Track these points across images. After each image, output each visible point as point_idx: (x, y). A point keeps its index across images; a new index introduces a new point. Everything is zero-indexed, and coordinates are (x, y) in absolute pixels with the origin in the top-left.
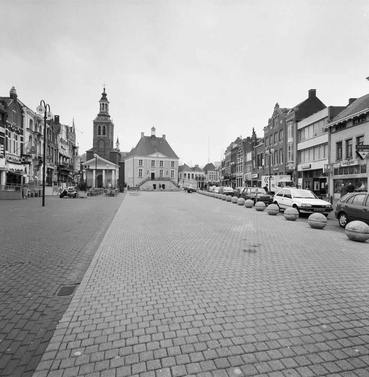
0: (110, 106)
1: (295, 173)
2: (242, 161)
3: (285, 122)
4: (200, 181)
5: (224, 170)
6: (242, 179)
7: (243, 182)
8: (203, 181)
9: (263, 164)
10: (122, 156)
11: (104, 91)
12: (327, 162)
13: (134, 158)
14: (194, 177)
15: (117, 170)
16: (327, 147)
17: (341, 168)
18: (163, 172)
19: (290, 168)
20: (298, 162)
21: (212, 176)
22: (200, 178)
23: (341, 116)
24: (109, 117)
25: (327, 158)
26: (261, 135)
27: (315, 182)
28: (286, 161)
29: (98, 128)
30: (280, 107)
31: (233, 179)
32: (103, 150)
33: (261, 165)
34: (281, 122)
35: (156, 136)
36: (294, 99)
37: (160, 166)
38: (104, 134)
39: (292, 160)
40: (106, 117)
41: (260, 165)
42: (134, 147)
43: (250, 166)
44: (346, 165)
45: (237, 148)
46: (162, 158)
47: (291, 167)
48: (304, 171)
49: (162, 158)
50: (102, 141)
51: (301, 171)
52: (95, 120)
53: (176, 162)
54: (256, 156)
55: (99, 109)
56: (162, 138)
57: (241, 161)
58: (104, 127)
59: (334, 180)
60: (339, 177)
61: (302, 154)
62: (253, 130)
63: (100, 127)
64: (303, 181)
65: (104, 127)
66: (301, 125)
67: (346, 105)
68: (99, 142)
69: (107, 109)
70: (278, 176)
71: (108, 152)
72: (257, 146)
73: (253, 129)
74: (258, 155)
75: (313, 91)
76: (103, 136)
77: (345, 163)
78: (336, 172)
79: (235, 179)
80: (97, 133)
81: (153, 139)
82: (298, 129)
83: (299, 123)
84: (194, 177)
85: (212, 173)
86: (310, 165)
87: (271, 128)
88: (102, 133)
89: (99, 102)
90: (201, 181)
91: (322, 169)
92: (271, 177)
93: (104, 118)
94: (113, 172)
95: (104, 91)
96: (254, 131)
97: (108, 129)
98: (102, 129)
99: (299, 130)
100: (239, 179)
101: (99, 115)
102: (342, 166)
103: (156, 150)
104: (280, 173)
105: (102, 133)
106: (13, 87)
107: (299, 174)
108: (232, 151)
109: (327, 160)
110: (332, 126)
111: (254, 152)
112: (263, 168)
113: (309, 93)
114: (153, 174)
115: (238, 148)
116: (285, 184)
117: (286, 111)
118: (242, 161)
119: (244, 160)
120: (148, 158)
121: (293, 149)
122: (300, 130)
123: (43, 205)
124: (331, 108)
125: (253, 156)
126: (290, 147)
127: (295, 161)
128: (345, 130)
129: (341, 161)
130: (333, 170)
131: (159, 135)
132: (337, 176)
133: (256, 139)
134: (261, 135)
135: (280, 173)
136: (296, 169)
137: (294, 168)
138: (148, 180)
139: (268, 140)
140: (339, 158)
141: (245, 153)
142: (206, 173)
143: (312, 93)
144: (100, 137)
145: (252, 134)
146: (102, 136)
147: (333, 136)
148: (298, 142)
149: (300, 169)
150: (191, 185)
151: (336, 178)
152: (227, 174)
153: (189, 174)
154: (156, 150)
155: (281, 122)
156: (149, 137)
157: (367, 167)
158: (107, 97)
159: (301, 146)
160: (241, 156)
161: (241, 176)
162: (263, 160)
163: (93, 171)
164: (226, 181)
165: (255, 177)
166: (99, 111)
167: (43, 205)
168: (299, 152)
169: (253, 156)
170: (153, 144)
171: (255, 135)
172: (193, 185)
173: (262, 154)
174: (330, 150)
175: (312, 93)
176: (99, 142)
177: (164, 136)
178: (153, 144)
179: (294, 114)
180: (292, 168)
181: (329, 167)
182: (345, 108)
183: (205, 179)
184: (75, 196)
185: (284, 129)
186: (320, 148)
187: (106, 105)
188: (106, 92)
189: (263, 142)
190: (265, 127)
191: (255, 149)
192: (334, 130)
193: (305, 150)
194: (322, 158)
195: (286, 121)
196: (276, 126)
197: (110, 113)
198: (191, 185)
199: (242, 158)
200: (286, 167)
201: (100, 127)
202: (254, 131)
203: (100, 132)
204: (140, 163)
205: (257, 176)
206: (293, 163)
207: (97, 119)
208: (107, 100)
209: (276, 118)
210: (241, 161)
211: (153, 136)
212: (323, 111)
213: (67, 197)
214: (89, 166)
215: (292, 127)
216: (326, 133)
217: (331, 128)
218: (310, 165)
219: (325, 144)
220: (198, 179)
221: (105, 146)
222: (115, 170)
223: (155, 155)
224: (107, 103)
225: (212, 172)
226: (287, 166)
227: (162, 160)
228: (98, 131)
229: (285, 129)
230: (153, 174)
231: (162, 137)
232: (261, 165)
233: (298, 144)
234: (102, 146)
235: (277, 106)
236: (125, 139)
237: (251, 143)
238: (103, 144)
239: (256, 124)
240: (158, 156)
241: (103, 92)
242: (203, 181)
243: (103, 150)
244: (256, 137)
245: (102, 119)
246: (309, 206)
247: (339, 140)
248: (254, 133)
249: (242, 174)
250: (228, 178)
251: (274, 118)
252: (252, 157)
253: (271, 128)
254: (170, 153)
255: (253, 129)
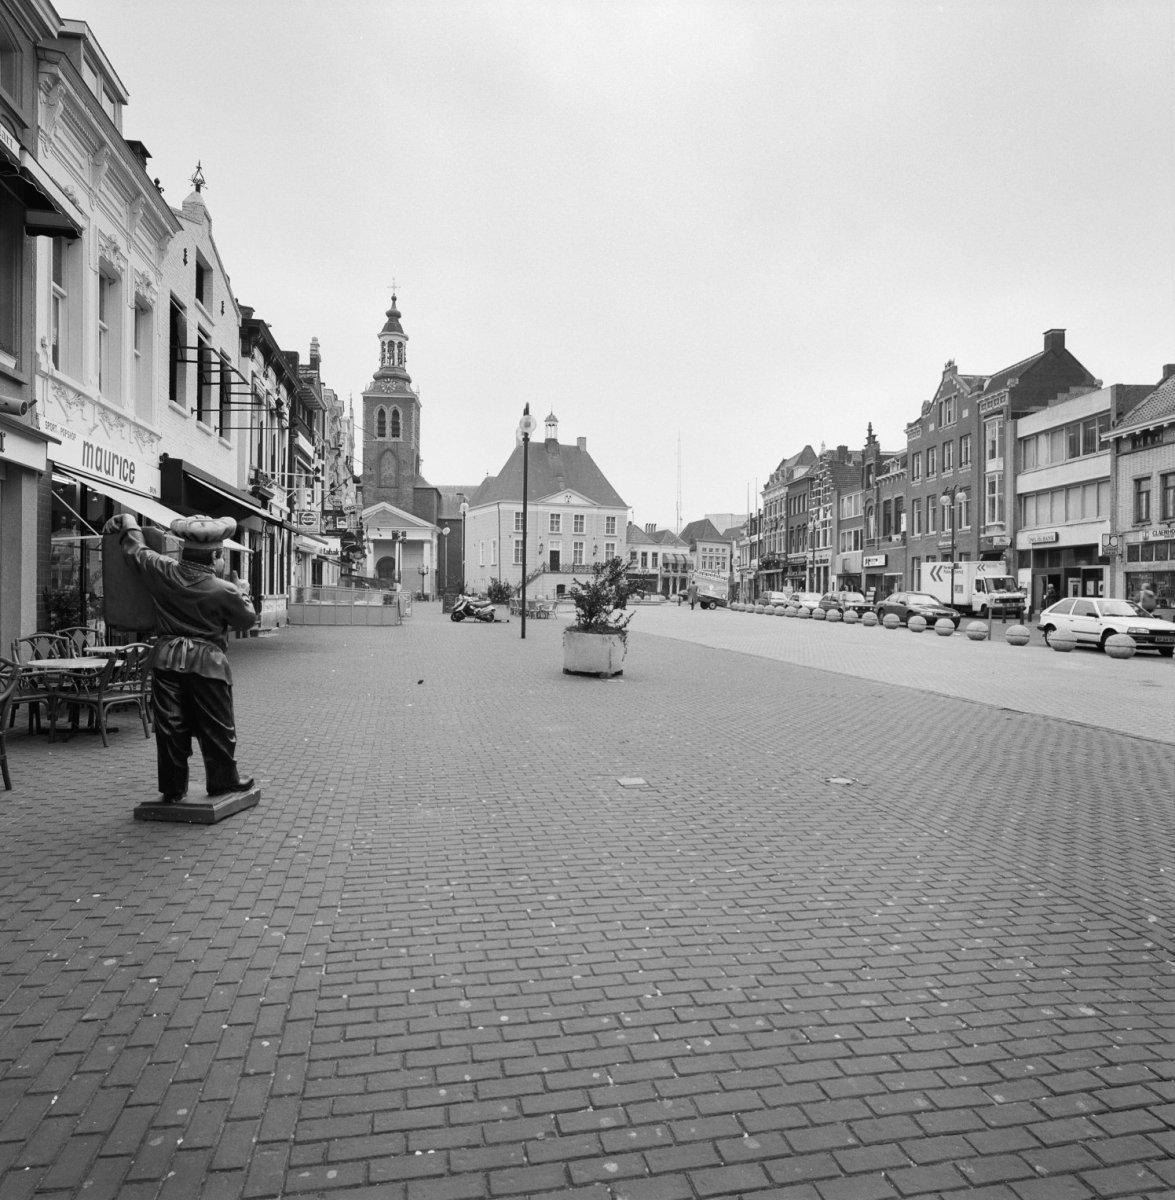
0: (409, 346)
1: (1008, 553)
2: (829, 517)
3: (979, 416)
4: (675, 575)
5: (760, 541)
6: (826, 568)
7: (833, 579)
8: (684, 575)
9: (904, 528)
10: (443, 498)
11: (394, 304)
12: (1107, 528)
13: (502, 506)
14: (660, 562)
15: (435, 541)
16: (1106, 490)
17: (1148, 544)
18: (584, 549)
19: (996, 542)
20: (1019, 525)
21: (711, 557)
22: (675, 566)
23: (1146, 412)
24: (408, 380)
25: (1106, 515)
26: (894, 442)
27: (1070, 579)
28: (981, 520)
29: (376, 417)
30: (960, 372)
31: (795, 568)
32: (392, 483)
33: (897, 531)
34: (966, 414)
35: (561, 442)
36: (1002, 347)
37: (576, 530)
38: (396, 433)
39: (1002, 518)
40: (400, 383)
41: (893, 530)
42: (495, 473)
43: (856, 533)
44: (1162, 538)
45: (809, 480)
46: (578, 506)
47: (999, 537)
48: (1035, 551)
49: (578, 506)
50: (388, 455)
51: (1028, 551)
52: (370, 391)
53: (621, 517)
54: (878, 506)
55: (379, 356)
56: (577, 448)
57: (825, 516)
58: (396, 414)
59: (1128, 574)
60: (1142, 566)
61: (1031, 504)
62: (870, 430)
63: (382, 413)
64: (1033, 576)
65: (396, 414)
66: (1027, 426)
67: (1154, 382)
68: (381, 456)
69: (402, 360)
70: (974, 564)
71: (408, 489)
72: (884, 477)
73: (870, 426)
74: (887, 503)
75: (1058, 335)
76: (394, 440)
77: (1161, 533)
78: (1133, 553)
79: (804, 568)
80: (376, 431)
81: (552, 450)
82: (1020, 435)
83: (1021, 422)
84: (660, 562)
85: (711, 550)
86: (1057, 535)
87: (932, 427)
88: (388, 430)
89: (380, 336)
90: (679, 574)
91: (1096, 546)
92: (956, 566)
93: (393, 385)
94: (427, 547)
95: (394, 304)
96: (873, 433)
97: (408, 418)
98: (388, 418)
99: (1020, 439)
100: (819, 569)
101: (377, 378)
102: (1152, 538)
103: (562, 485)
104: (961, 554)
105: (388, 430)
106: (315, 339)
107: (1022, 558)
108: (791, 486)
109: (1108, 523)
110: (1124, 436)
111: (872, 494)
112: (904, 540)
113: (1046, 339)
114: (555, 555)
115: (813, 479)
116: (992, 586)
117: (975, 383)
118: (829, 517)
119: (835, 514)
120: (540, 508)
121: (1003, 489)
122: (1025, 440)
123: (523, 636)
124: (1121, 391)
125: (869, 505)
126: (992, 484)
127: (1008, 523)
128: (1159, 449)
129: (1147, 527)
130: (1125, 548)
131: (566, 438)
132: (1134, 563)
133: (880, 458)
134: (894, 442)
135: (961, 554)
136: (1013, 544)
137: (1008, 541)
138: (544, 571)
139: (920, 463)
140: (1141, 520)
141: (839, 495)
142: (693, 550)
143: (1055, 339)
144: (384, 443)
145: (866, 442)
146: (388, 438)
147: (1124, 461)
148: (1017, 473)
149: (1024, 542)
150: (711, 587)
151: (1132, 570)
152: (773, 554)
153: (644, 554)
154: (562, 485)
155: (966, 414)
156: (539, 444)
157: (1083, 496)
158: (400, 320)
159: (1027, 483)
160: (826, 502)
161: (826, 561)
162: (903, 515)
163: (422, 547)
164: (768, 575)
165: (877, 564)
166: (379, 364)
167: (523, 636)
168: (1021, 499)
169: (869, 505)
170: (545, 466)
171: (876, 444)
172: (718, 588)
173: (899, 500)
174: (1115, 497)
175: (1055, 339)
176: (381, 456)
177: (582, 440)
178: (545, 466)
179: (1007, 395)
180: (1002, 540)
181: (1114, 542)
182: (1155, 388)
183: (691, 566)
184: (488, 618)
185: (972, 432)
186: (1084, 492)
187: (400, 345)
188: (399, 308)
189: (904, 465)
190: (910, 425)
191: (877, 484)
192: (1127, 447)
193: (1038, 493)
194: (1091, 516)
195: (982, 412)
196: (949, 425)
197: (410, 369)
198: (711, 587)
199: (826, 510)
200: (979, 539)
201: (382, 413)
202: (873, 433)
203: (384, 429)
204: (552, 522)
205: (881, 561)
206: (1002, 527)
207: (375, 388)
208: (402, 331)
209: (946, 401)
210: (825, 516)
211: (551, 443)
212: (1096, 395)
213: (473, 619)
214: (404, 534)
215: (1002, 431)
216: (1103, 452)
217: (1118, 441)
218: (1057, 535)
219: (1098, 482)
220: (670, 568)
221: (398, 471)
222: (430, 542)
223: (560, 499)
224: (402, 340)
225: (708, 546)
226: (982, 536)
227: (580, 512)
228: (376, 425)
229: (979, 434)
230: (555, 555)
231: (574, 443)
232: (897, 531)
233: (1020, 479)
234: (388, 470)
235: (951, 368)
236: (457, 452)
237: (857, 469)
238: (394, 462)
239: (883, 411)
240: (567, 502)
241: (389, 307)
242: (684, 575)
243: (392, 483)
244: (878, 452)
245: (389, 389)
246: (1143, 631)
247: (1140, 473)
248: (871, 438)
249: (827, 554)
250: (777, 565)
251: (943, 400)
252: (865, 508)
253: (932, 427)
254: (601, 492)
255: (870, 426)
